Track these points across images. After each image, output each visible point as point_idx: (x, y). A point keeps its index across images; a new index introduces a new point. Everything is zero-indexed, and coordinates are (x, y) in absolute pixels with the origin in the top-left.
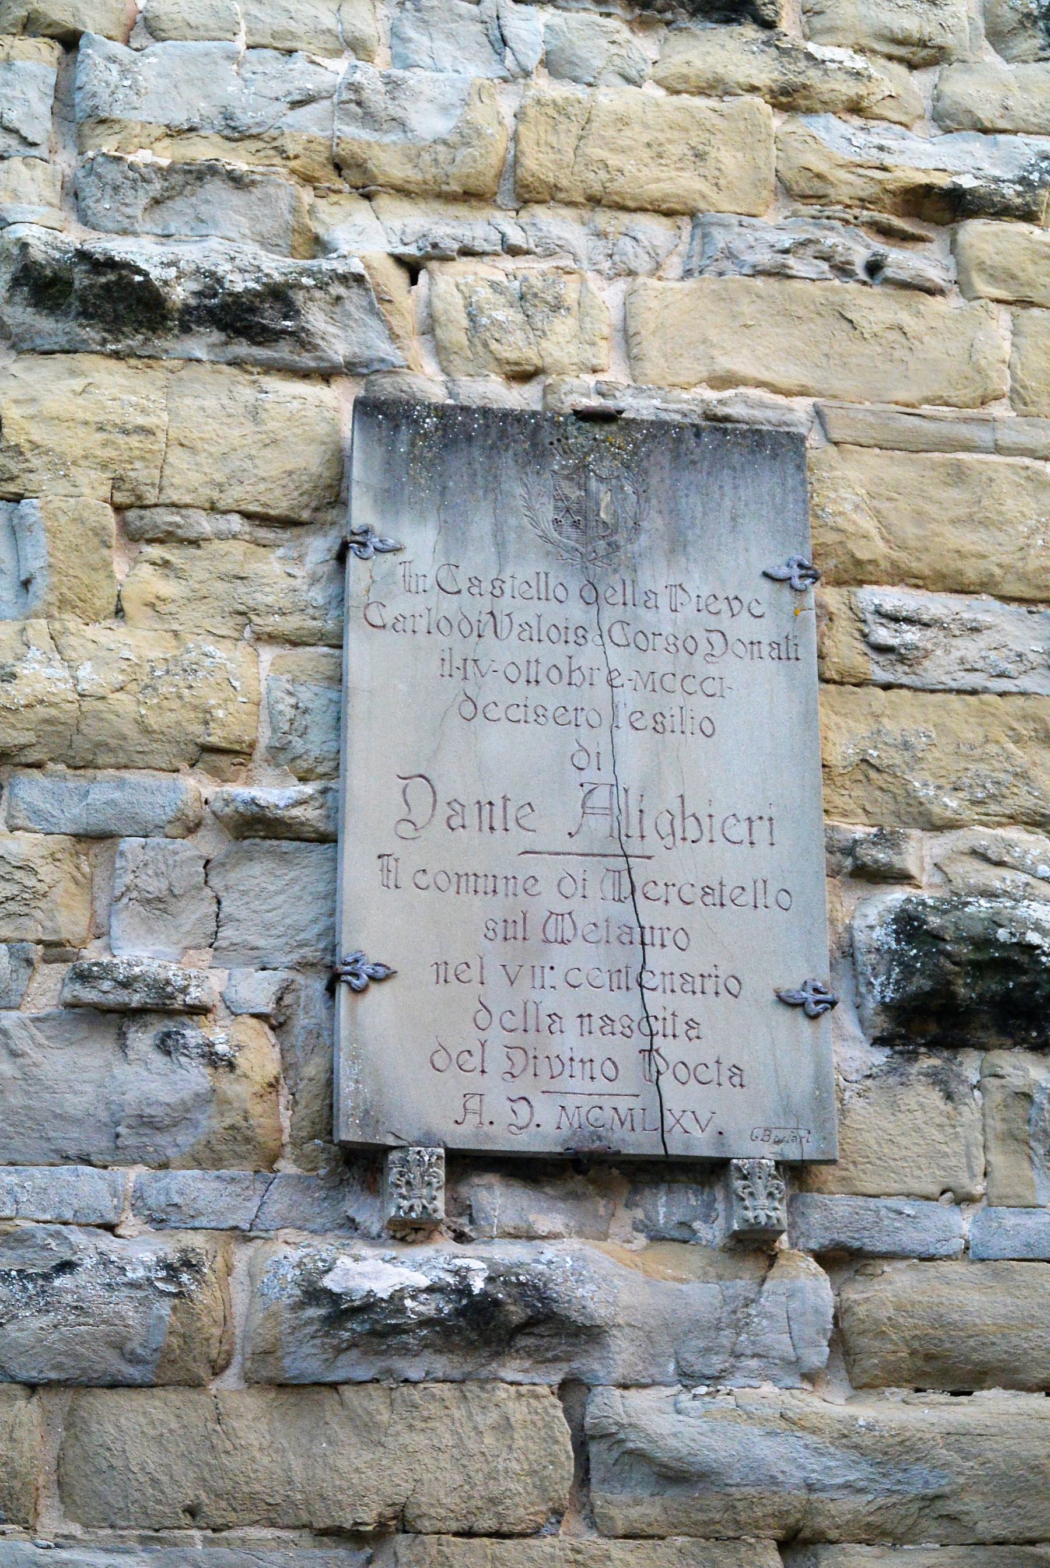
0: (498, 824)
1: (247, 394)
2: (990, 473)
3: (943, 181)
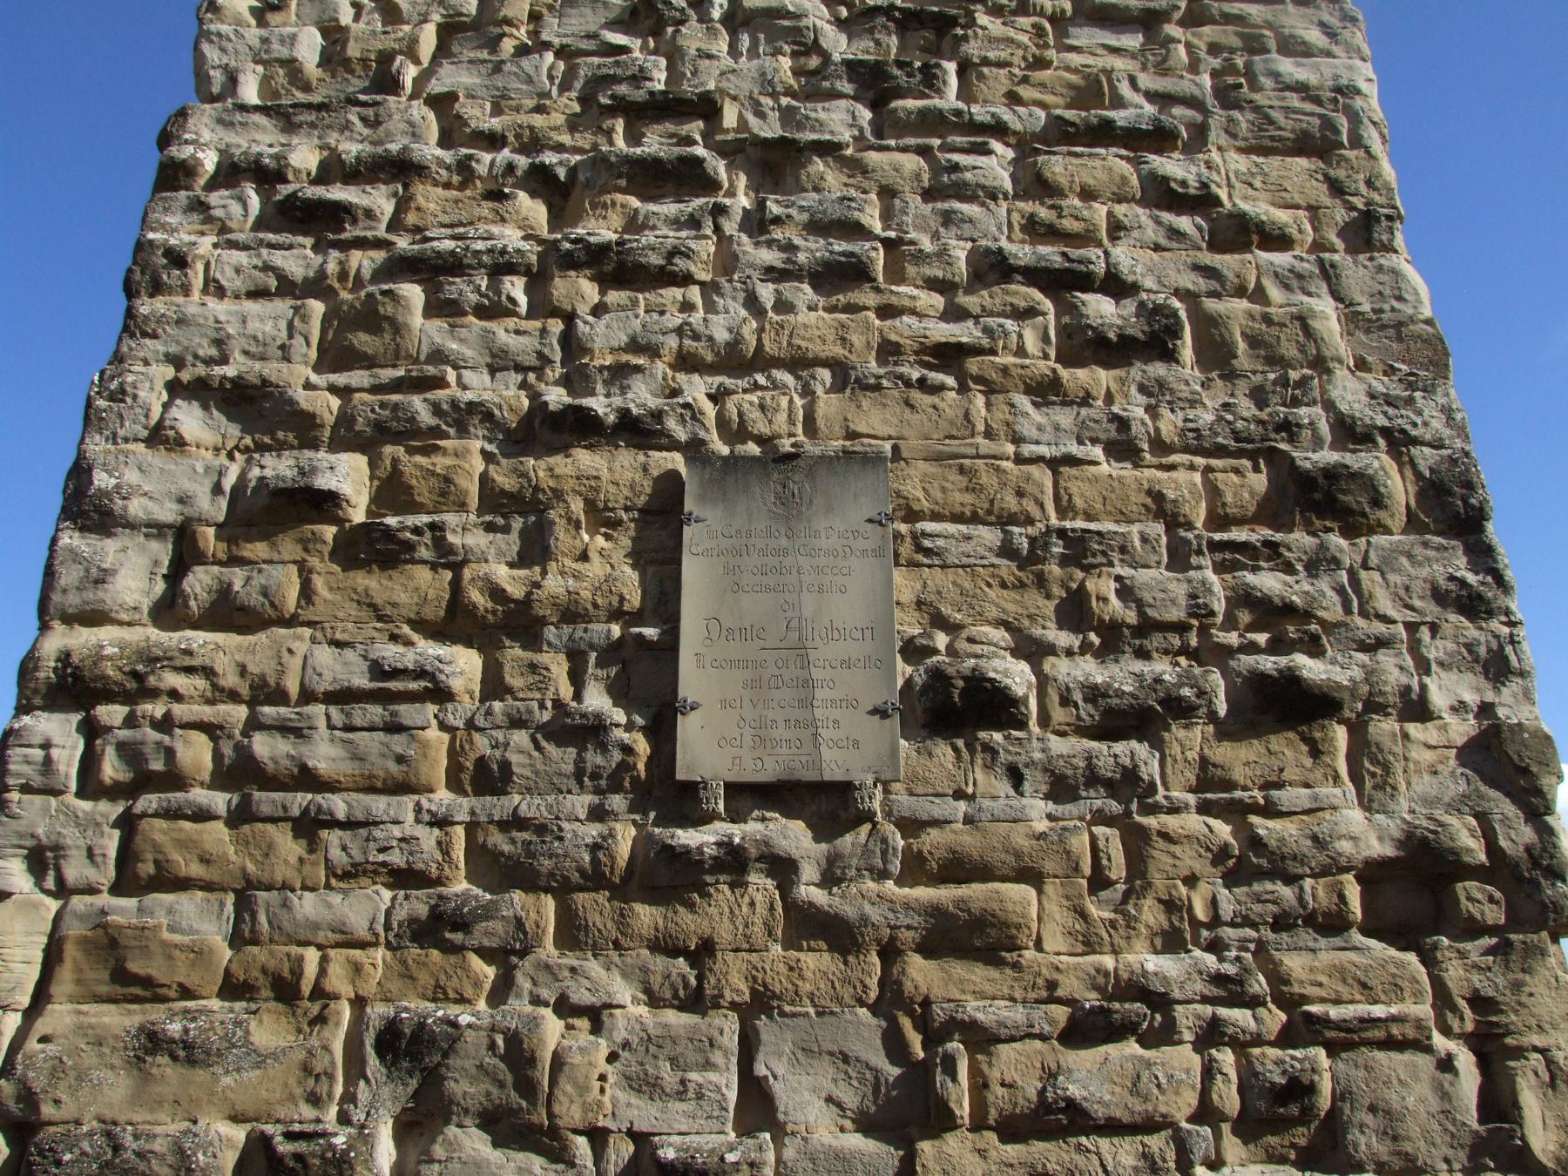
1: (641, 458)
3: (952, 340)
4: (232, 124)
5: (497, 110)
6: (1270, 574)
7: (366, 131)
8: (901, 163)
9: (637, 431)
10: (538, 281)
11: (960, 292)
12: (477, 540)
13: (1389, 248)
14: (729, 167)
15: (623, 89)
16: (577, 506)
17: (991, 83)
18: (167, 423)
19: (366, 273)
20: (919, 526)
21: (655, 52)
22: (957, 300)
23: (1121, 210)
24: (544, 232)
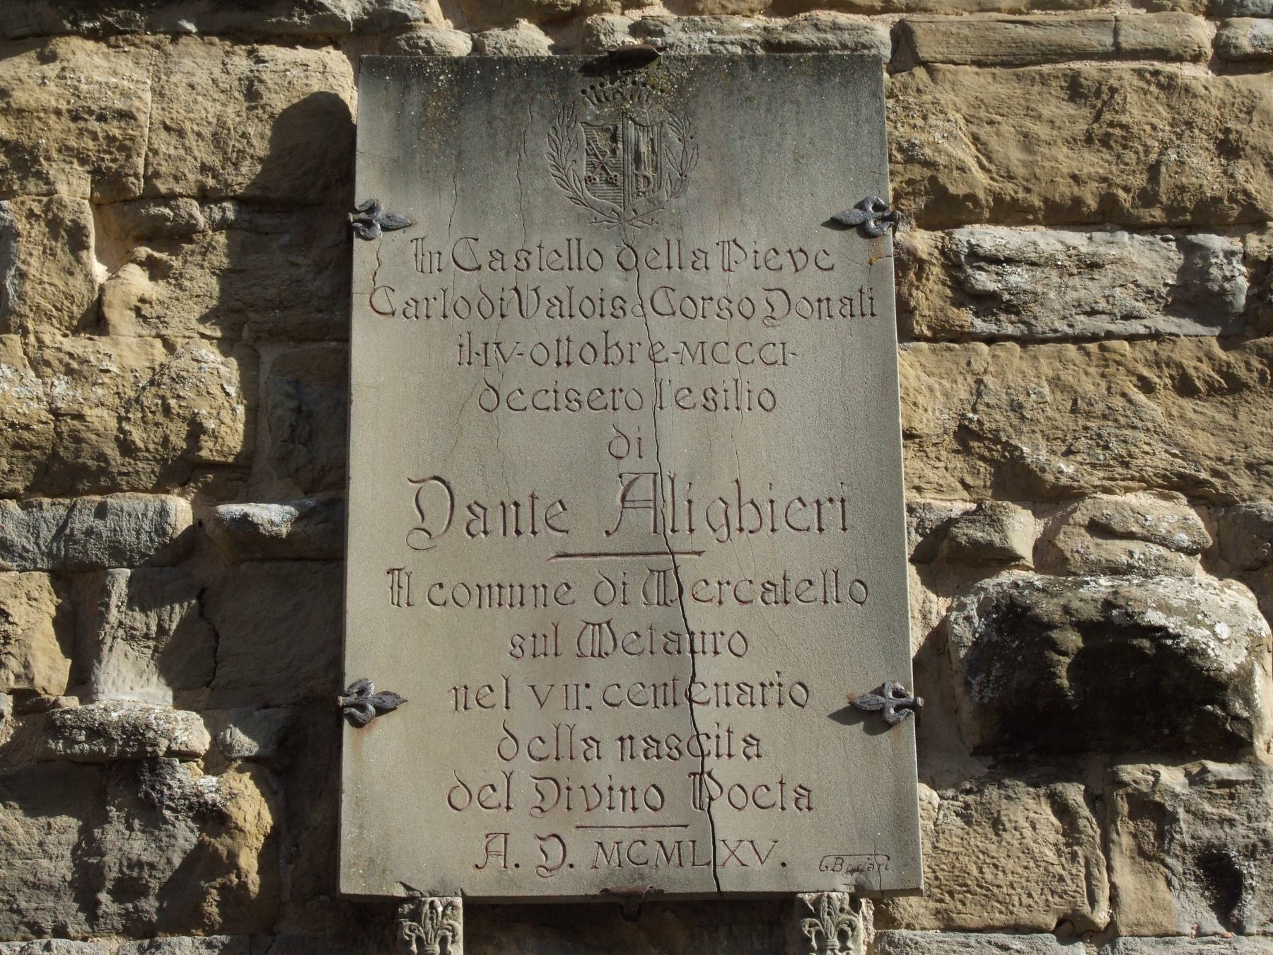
0: (525, 526)
1: (241, 63)
2: (1111, 81)
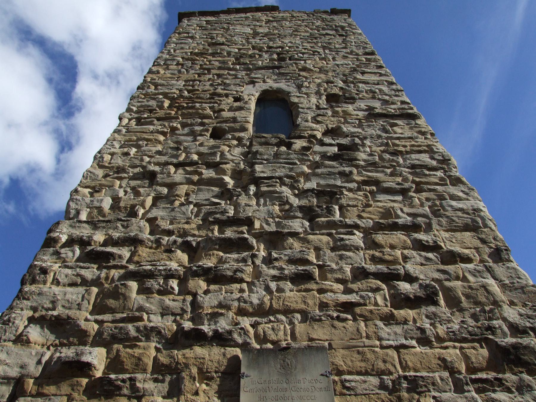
3: (349, 301)
4: (75, 227)
5: (171, 223)
6: (501, 393)
7: (123, 230)
8: (322, 239)
9: (221, 339)
10: (183, 281)
11: (349, 283)
12: (150, 386)
13: (509, 261)
14: (257, 242)
15: (218, 216)
16: (194, 371)
17: (351, 212)
18: (24, 333)
19: (116, 277)
20: (343, 377)
21: (230, 205)
22: (348, 286)
23: (406, 252)
24: (187, 264)
